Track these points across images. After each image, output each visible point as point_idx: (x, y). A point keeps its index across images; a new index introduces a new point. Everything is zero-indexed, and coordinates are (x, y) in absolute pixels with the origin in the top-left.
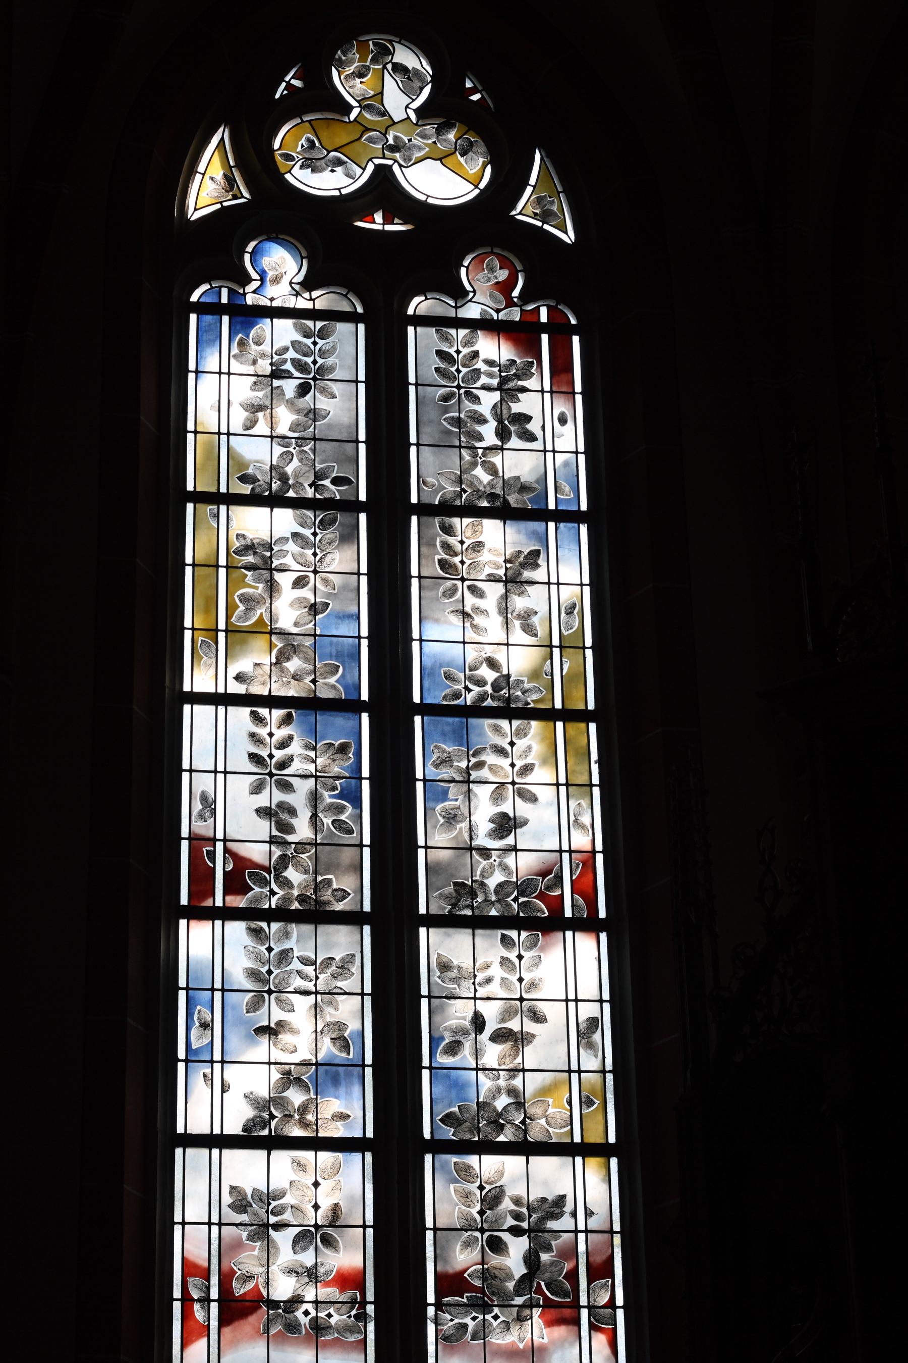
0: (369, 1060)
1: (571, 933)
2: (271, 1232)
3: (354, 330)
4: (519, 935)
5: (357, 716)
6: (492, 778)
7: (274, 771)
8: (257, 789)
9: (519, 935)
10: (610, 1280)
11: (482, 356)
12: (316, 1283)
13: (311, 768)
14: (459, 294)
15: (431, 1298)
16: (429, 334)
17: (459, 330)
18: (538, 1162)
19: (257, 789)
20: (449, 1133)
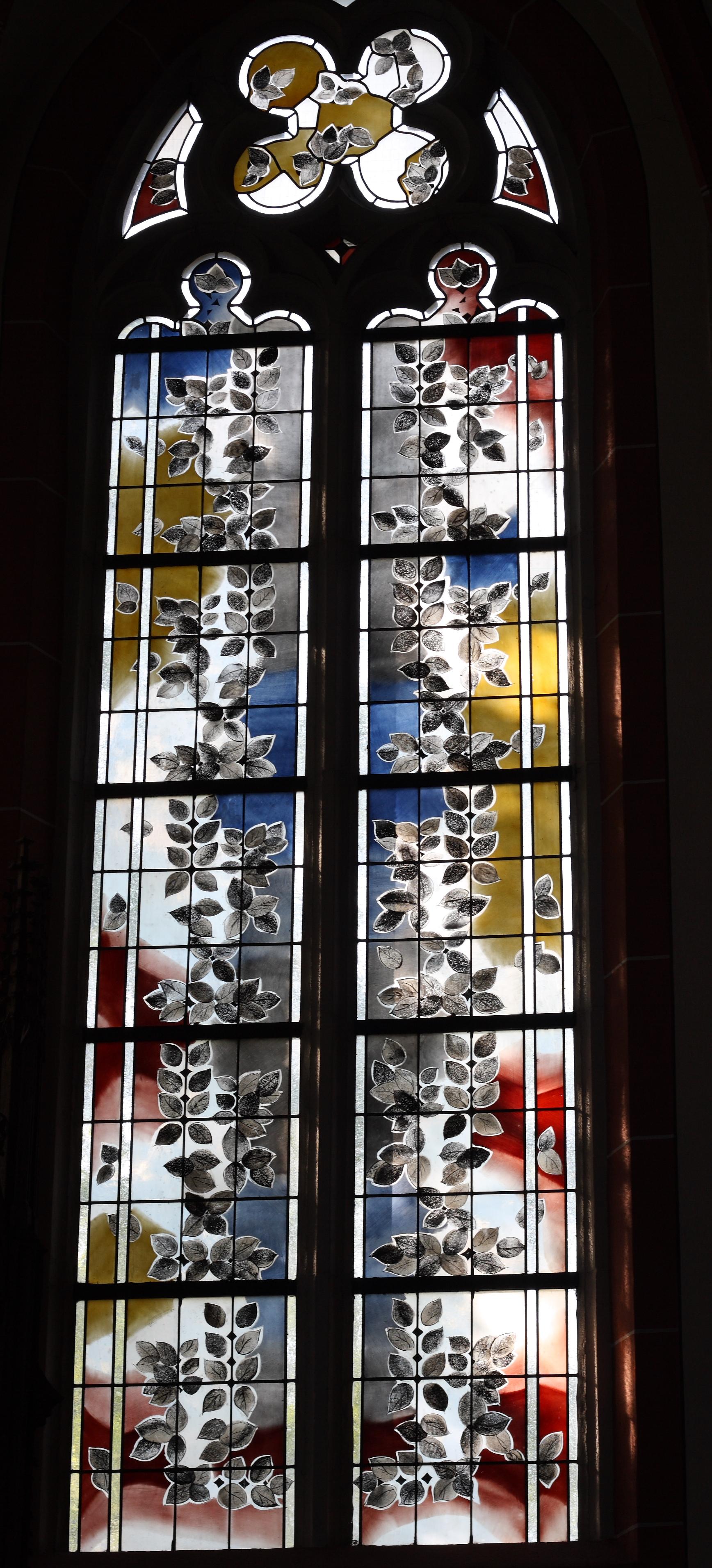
0: (298, 937)
1: (534, 1291)
2: (206, 488)
3: (283, 1389)
4: (472, 1037)
5: (292, 796)
6: (447, 1107)
7: (189, 1116)
8: (172, 888)
9: (472, 1037)
10: (560, 1434)
11: (448, 1334)
12: (248, 668)
13: (236, 859)
14: (425, 301)
15: (357, 1459)
16: (388, 352)
17: (421, 1295)
18: (483, 1298)
19: (172, 888)
20: (382, 1270)
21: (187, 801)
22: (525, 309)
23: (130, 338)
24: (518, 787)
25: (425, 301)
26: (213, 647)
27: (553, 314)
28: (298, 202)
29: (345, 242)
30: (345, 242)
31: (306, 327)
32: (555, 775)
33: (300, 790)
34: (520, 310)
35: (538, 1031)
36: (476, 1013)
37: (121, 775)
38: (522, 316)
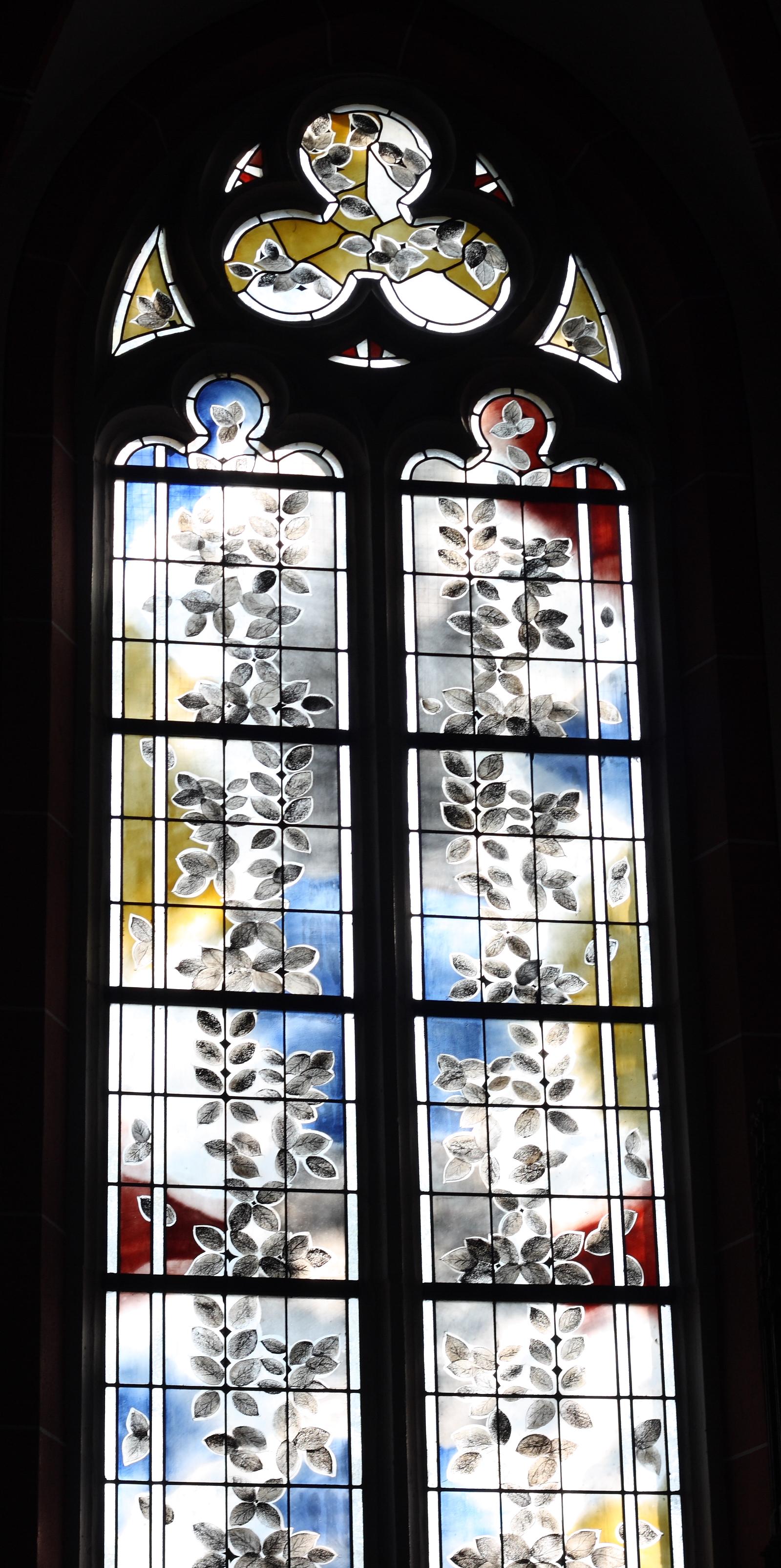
14: (467, 449)
21: (216, 1013)
22: (584, 468)
23: (129, 464)
24: (596, 1026)
25: (467, 449)
26: (242, 836)
27: (620, 486)
28: (310, 313)
29: (228, 189)
30: (228, 189)
31: (339, 474)
32: (638, 1016)
33: (350, 1012)
34: (578, 469)
35: (150, 986)
36: (557, 1283)
37: (137, 977)
38: (581, 482)
